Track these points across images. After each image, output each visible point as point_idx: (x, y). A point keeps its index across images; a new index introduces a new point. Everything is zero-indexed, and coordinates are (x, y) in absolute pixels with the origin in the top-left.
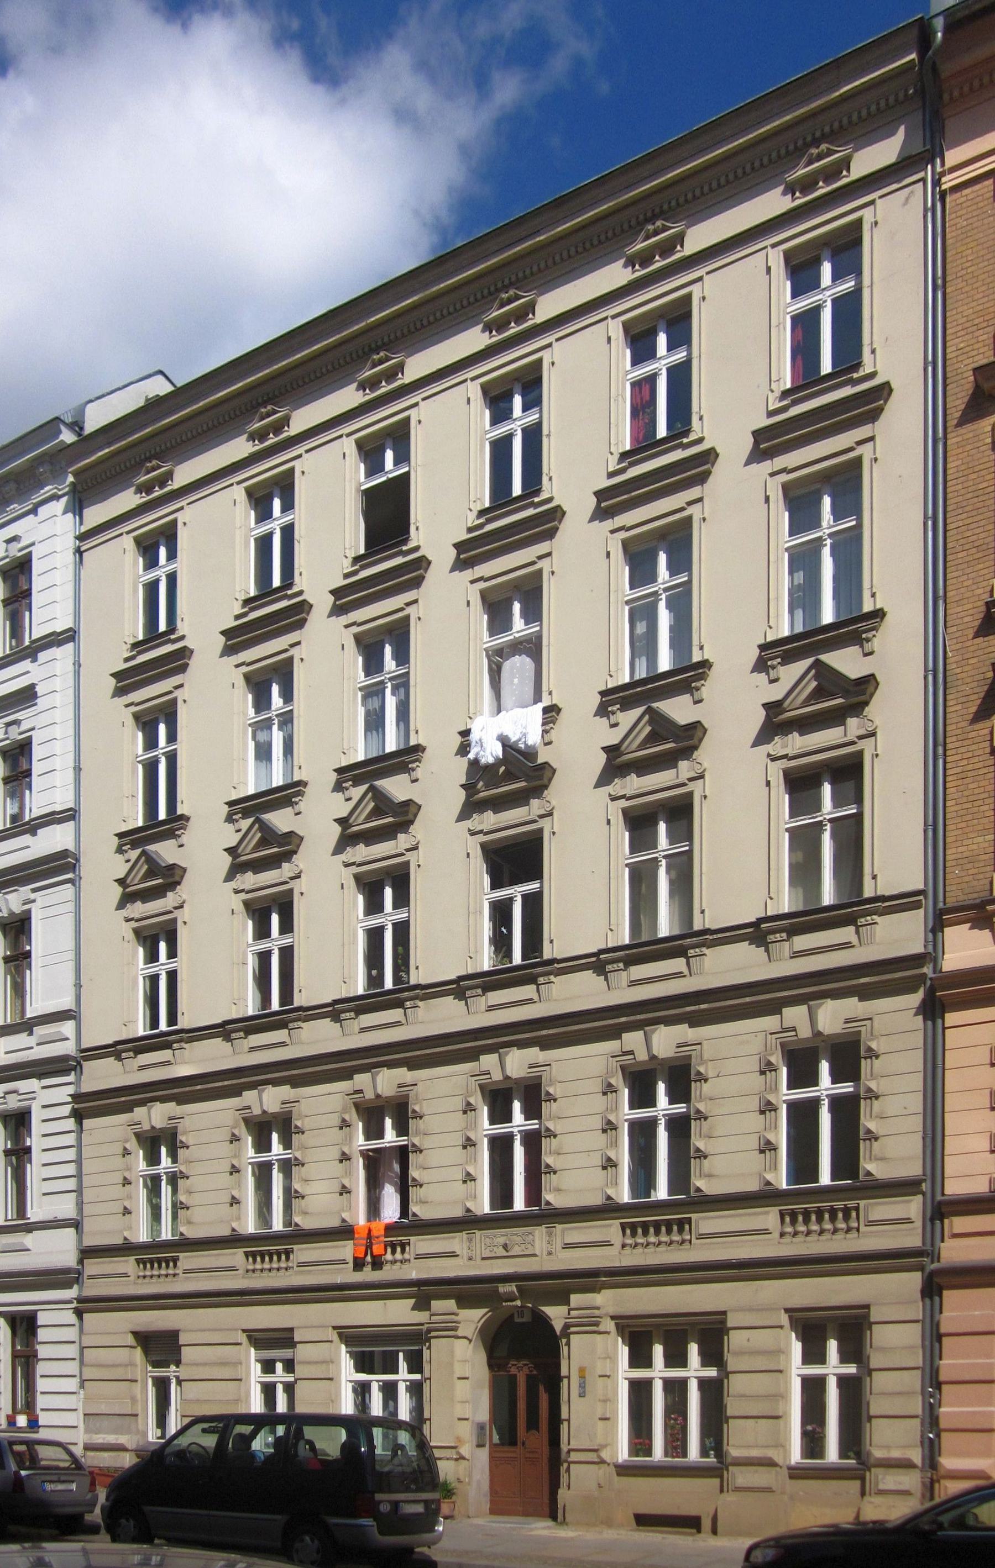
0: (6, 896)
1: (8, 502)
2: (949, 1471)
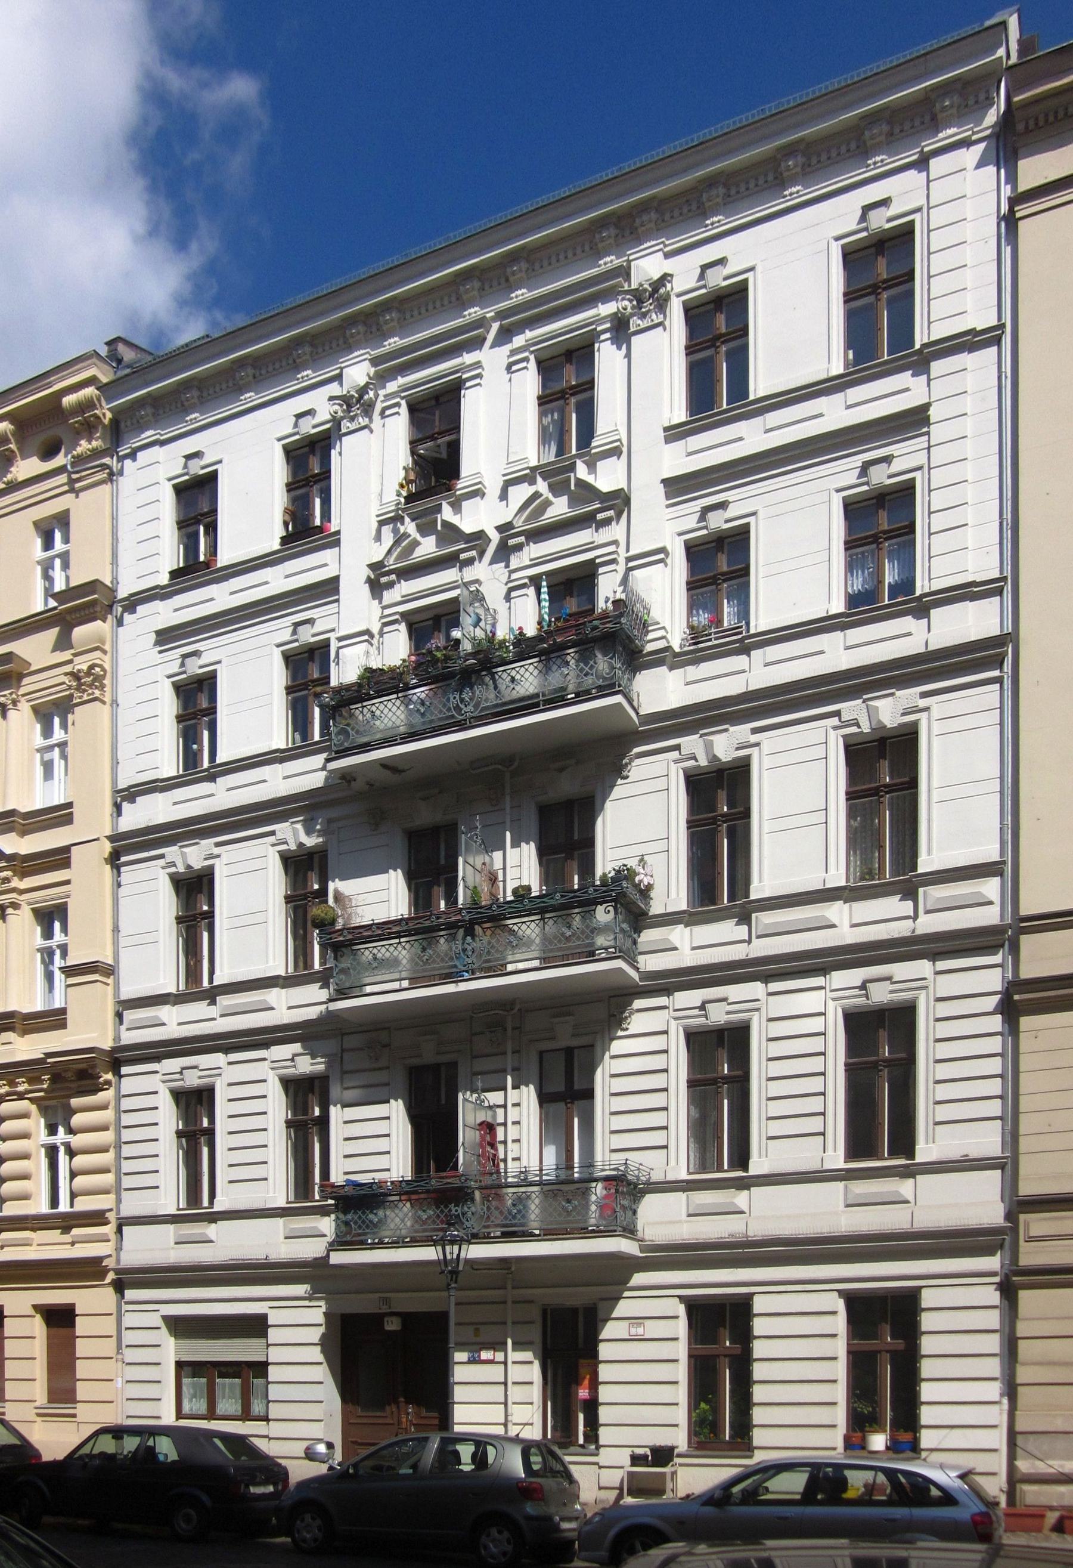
0: (184, 850)
1: (187, 410)
2: (1024, 1474)
